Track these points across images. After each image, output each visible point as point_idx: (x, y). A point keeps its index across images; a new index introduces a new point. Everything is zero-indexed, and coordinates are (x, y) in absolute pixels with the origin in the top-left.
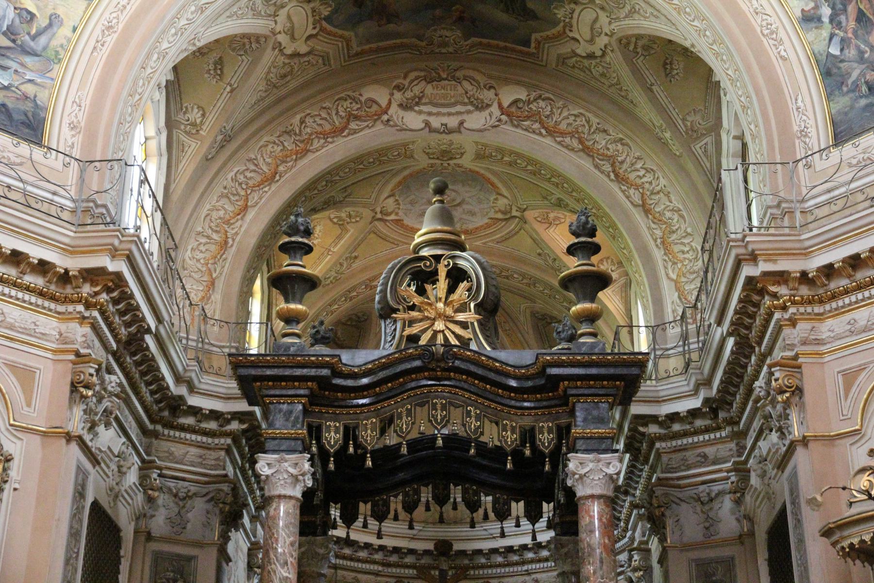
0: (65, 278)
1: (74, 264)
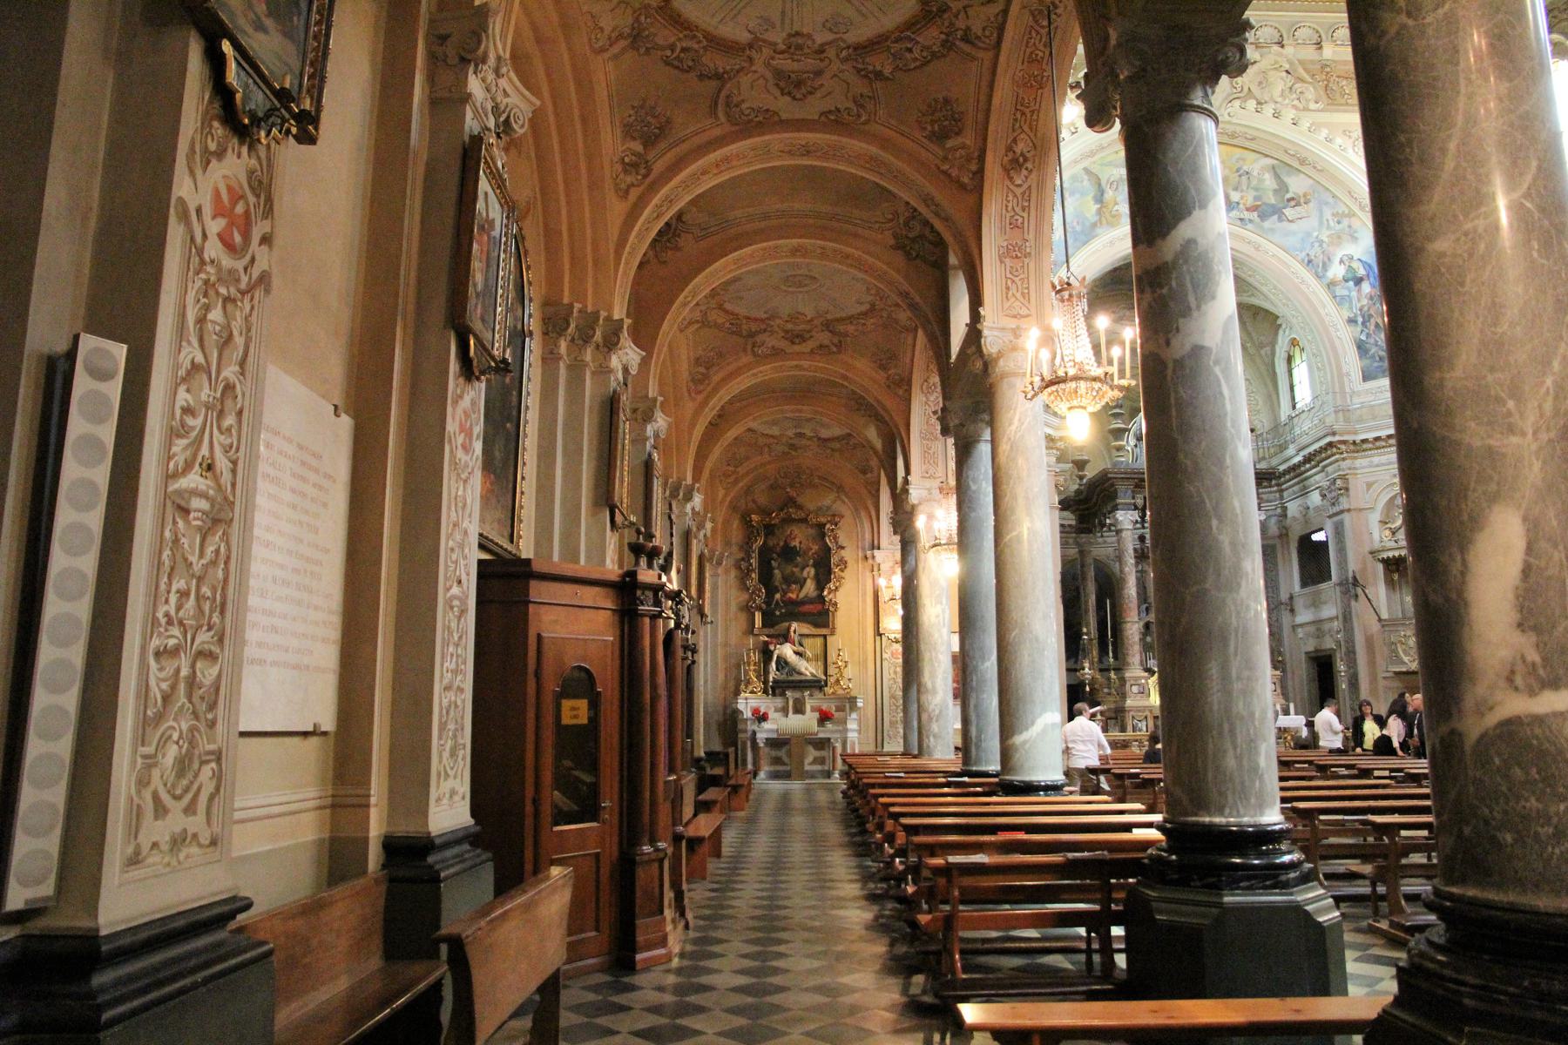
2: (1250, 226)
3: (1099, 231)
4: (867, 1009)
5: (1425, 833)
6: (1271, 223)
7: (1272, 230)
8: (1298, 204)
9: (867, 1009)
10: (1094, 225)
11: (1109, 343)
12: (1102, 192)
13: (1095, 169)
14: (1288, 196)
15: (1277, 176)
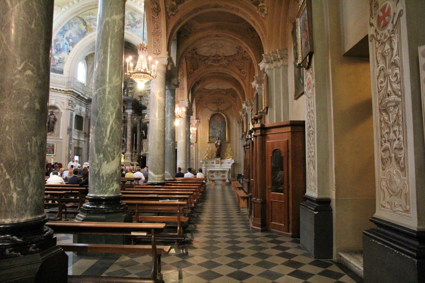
0: (66, 91)
1: (67, 90)
2: (129, 30)
3: (87, 33)
4: (201, 256)
5: (145, 234)
6: (134, 29)
7: (135, 31)
8: (139, 23)
9: (201, 256)
10: (85, 32)
11: (151, 64)
12: (86, 23)
13: (80, 16)
14: (136, 21)
15: (132, 16)
